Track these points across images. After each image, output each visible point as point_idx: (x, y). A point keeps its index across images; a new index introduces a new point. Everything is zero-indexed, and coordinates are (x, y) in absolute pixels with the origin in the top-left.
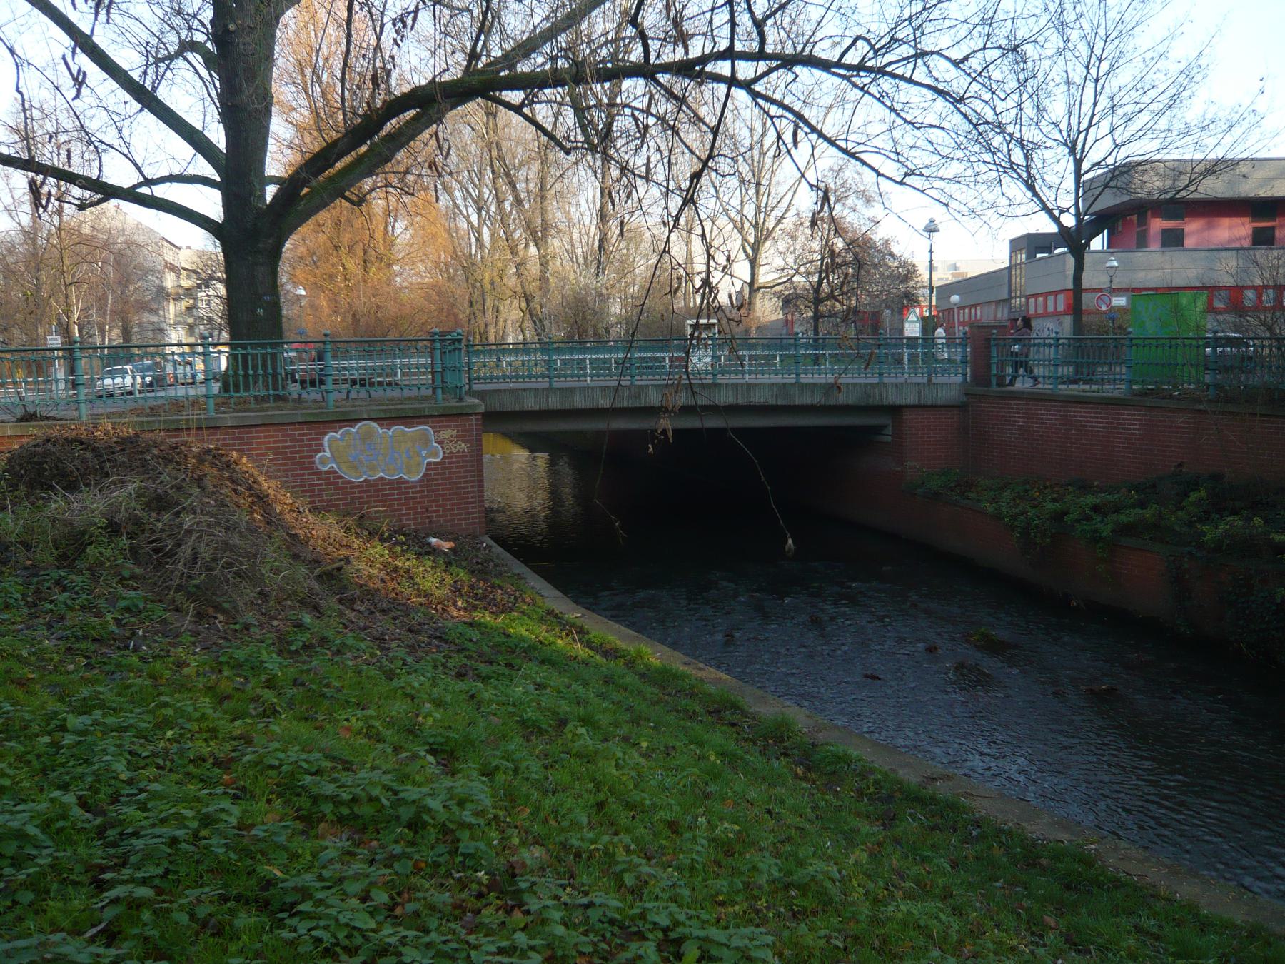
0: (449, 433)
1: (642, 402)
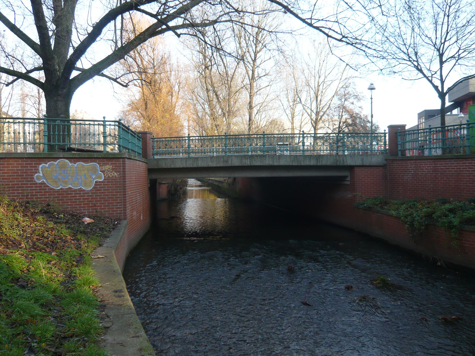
0: (108, 167)
1: (229, 164)
